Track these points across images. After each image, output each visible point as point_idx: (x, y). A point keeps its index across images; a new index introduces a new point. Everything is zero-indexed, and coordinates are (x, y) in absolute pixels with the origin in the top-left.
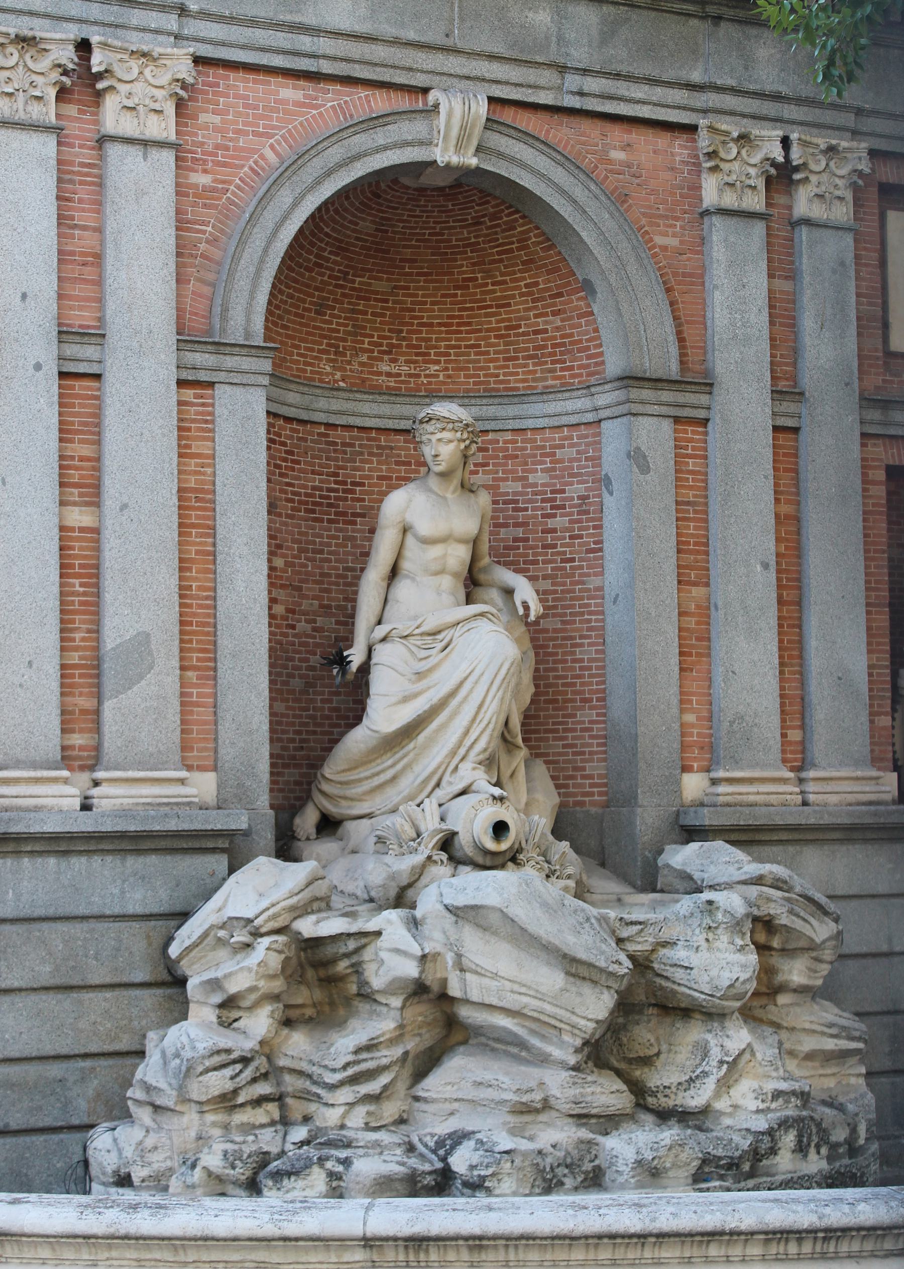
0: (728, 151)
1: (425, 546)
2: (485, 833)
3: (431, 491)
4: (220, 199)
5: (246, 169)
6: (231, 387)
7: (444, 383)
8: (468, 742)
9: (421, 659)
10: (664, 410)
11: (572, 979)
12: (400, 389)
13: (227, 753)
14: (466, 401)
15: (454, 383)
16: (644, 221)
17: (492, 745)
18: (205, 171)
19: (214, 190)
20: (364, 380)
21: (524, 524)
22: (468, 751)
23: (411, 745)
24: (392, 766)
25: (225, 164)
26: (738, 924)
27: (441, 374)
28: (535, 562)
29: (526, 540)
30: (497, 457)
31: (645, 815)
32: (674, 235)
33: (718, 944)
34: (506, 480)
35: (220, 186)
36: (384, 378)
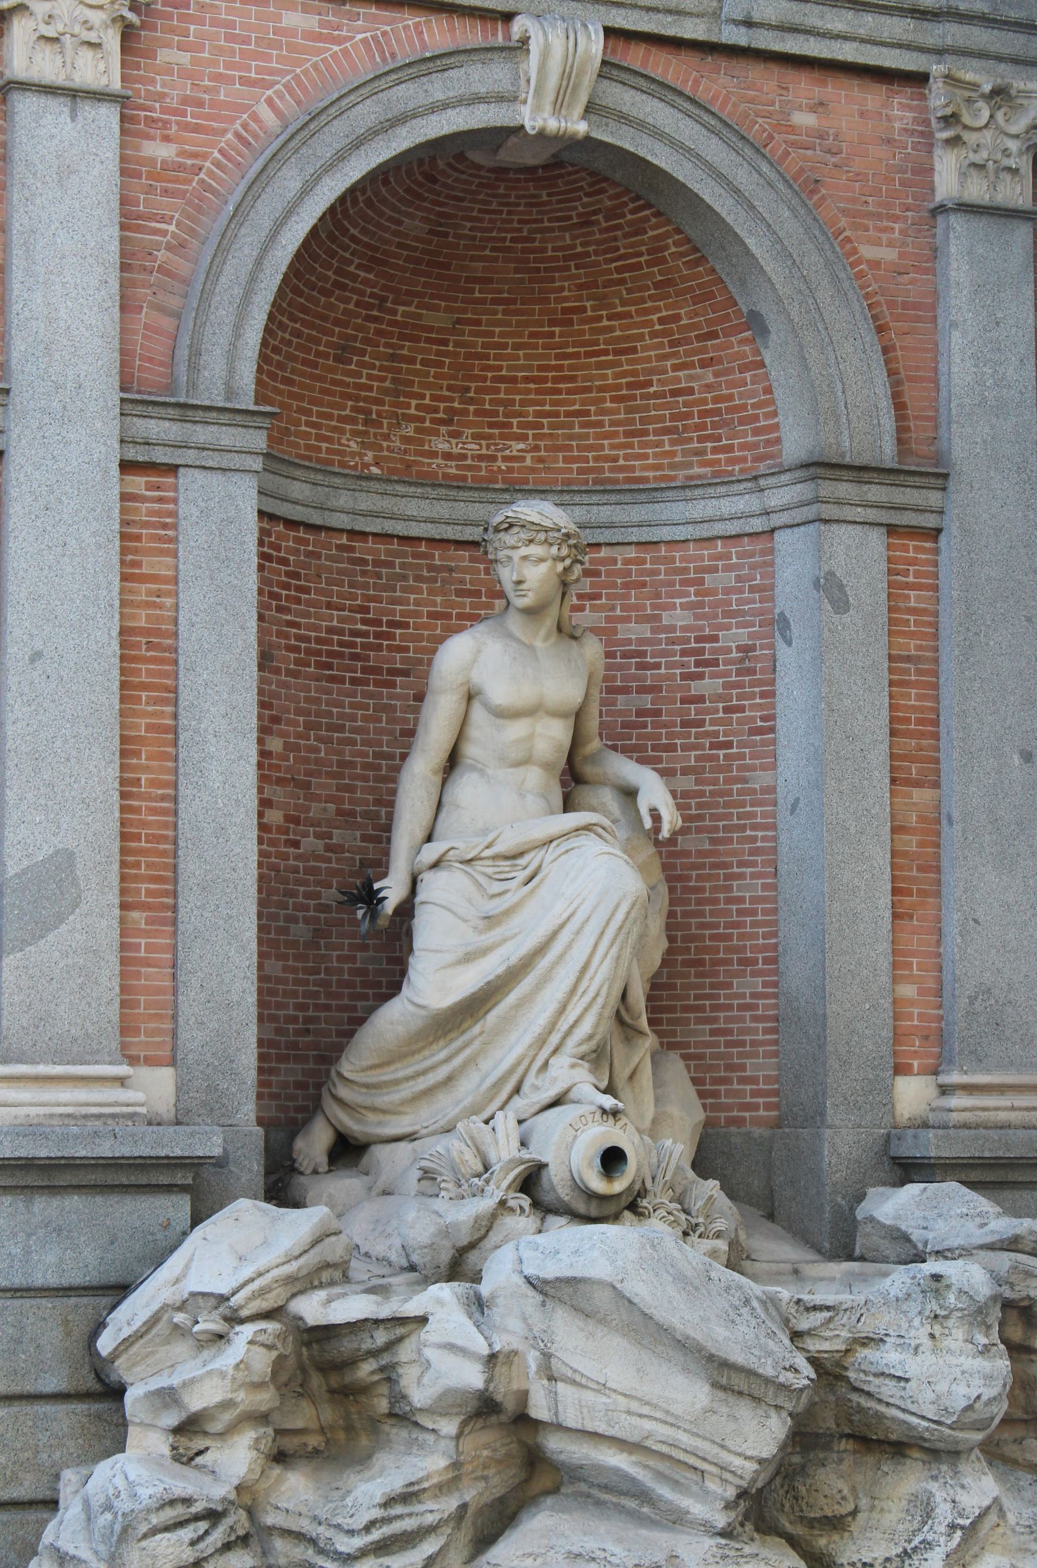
0: (976, 115)
1: (500, 721)
2: (590, 1165)
3: (510, 636)
4: (189, 182)
5: (230, 136)
6: (204, 473)
7: (533, 470)
8: (564, 1025)
9: (493, 896)
10: (872, 515)
11: (721, 1395)
12: (464, 478)
13: (191, 1038)
14: (567, 498)
15: (548, 470)
16: (843, 222)
17: (601, 1029)
18: (166, 139)
19: (180, 167)
20: (409, 465)
21: (654, 689)
22: (564, 1039)
23: (477, 1029)
24: (447, 1060)
25: (197, 129)
26: (979, 1311)
27: (529, 456)
28: (671, 748)
29: (658, 713)
30: (614, 585)
31: (837, 1140)
32: (890, 244)
33: (948, 1342)
34: (627, 620)
35: (189, 162)
36: (440, 461)
